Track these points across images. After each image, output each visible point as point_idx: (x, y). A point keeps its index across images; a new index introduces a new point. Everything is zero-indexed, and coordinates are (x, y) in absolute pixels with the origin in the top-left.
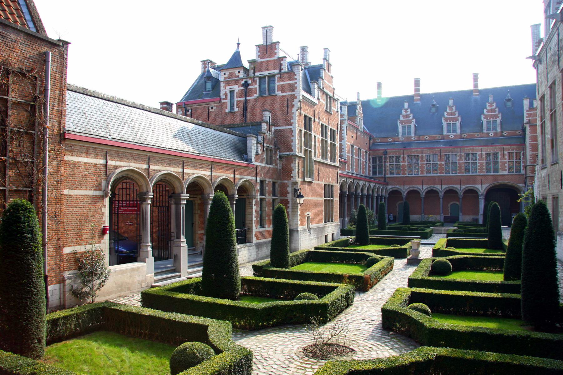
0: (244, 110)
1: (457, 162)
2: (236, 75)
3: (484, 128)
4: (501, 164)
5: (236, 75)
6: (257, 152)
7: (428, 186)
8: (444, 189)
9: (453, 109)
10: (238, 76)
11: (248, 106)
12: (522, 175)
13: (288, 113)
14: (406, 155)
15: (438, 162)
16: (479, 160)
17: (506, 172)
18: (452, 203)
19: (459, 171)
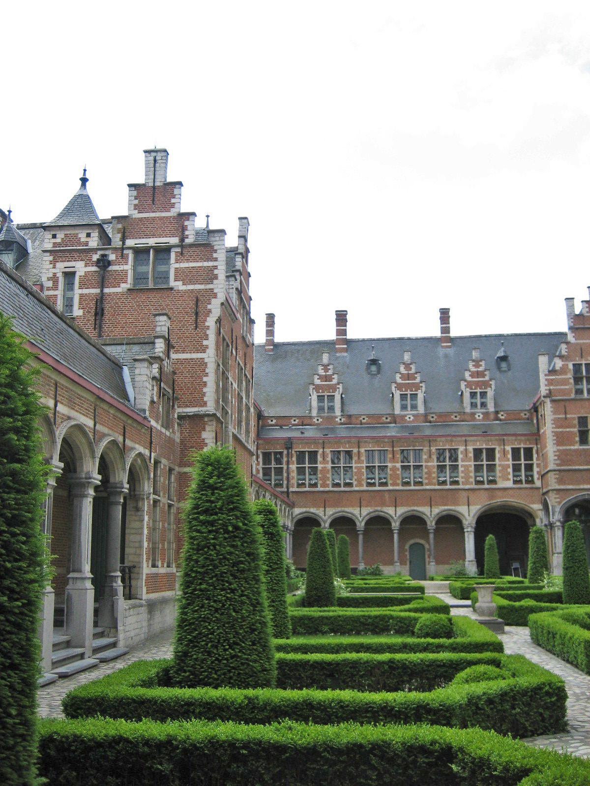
0: (96, 314)
1: (423, 464)
2: (82, 240)
3: (465, 405)
4: (500, 468)
5: (82, 240)
6: (152, 398)
7: (370, 509)
9: (411, 369)
10: (87, 244)
11: (107, 307)
12: (538, 488)
13: (196, 327)
14: (328, 451)
16: (462, 461)
17: (509, 484)
18: (412, 541)
19: (426, 481)
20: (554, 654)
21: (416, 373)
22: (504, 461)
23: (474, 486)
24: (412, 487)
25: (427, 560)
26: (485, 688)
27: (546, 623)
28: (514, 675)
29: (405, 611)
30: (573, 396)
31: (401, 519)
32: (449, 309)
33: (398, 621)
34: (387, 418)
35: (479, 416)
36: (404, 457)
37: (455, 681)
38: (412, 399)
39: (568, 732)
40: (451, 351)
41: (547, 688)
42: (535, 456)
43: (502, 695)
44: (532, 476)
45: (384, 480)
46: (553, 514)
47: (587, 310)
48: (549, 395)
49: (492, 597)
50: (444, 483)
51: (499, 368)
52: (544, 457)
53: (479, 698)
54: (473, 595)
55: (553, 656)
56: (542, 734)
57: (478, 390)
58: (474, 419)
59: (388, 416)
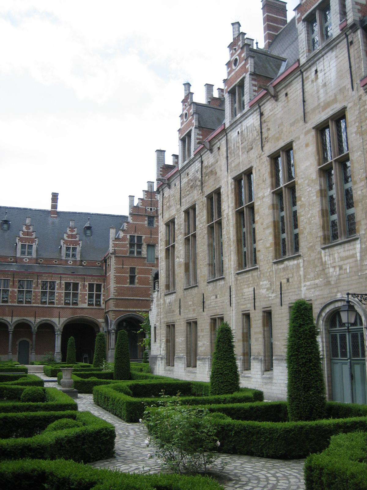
4: (81, 295)
8: (16, 322)
9: (30, 229)
15: (10, 289)
17: (86, 306)
18: (21, 339)
19: (34, 301)
20: (108, 411)
21: (33, 232)
22: (83, 292)
23: (63, 306)
24: (24, 305)
25: (30, 351)
26: (66, 433)
27: (104, 391)
28: (84, 424)
29: (15, 384)
30: (128, 255)
31: (15, 324)
32: (58, 194)
33: (10, 391)
34: (11, 259)
35: (70, 262)
36: (20, 285)
37: (47, 429)
38: (73, 251)
39: (115, 457)
40: (56, 220)
41: (104, 431)
42: (102, 289)
43: (77, 437)
44: (100, 302)
45: (6, 299)
46: (111, 326)
47: (141, 204)
48: (114, 253)
49: (71, 375)
50: (45, 303)
51: (85, 234)
52: (108, 290)
53: (62, 439)
54: (59, 374)
55: (107, 412)
56: (99, 460)
57: (71, 246)
58: (67, 264)
59: (12, 258)
